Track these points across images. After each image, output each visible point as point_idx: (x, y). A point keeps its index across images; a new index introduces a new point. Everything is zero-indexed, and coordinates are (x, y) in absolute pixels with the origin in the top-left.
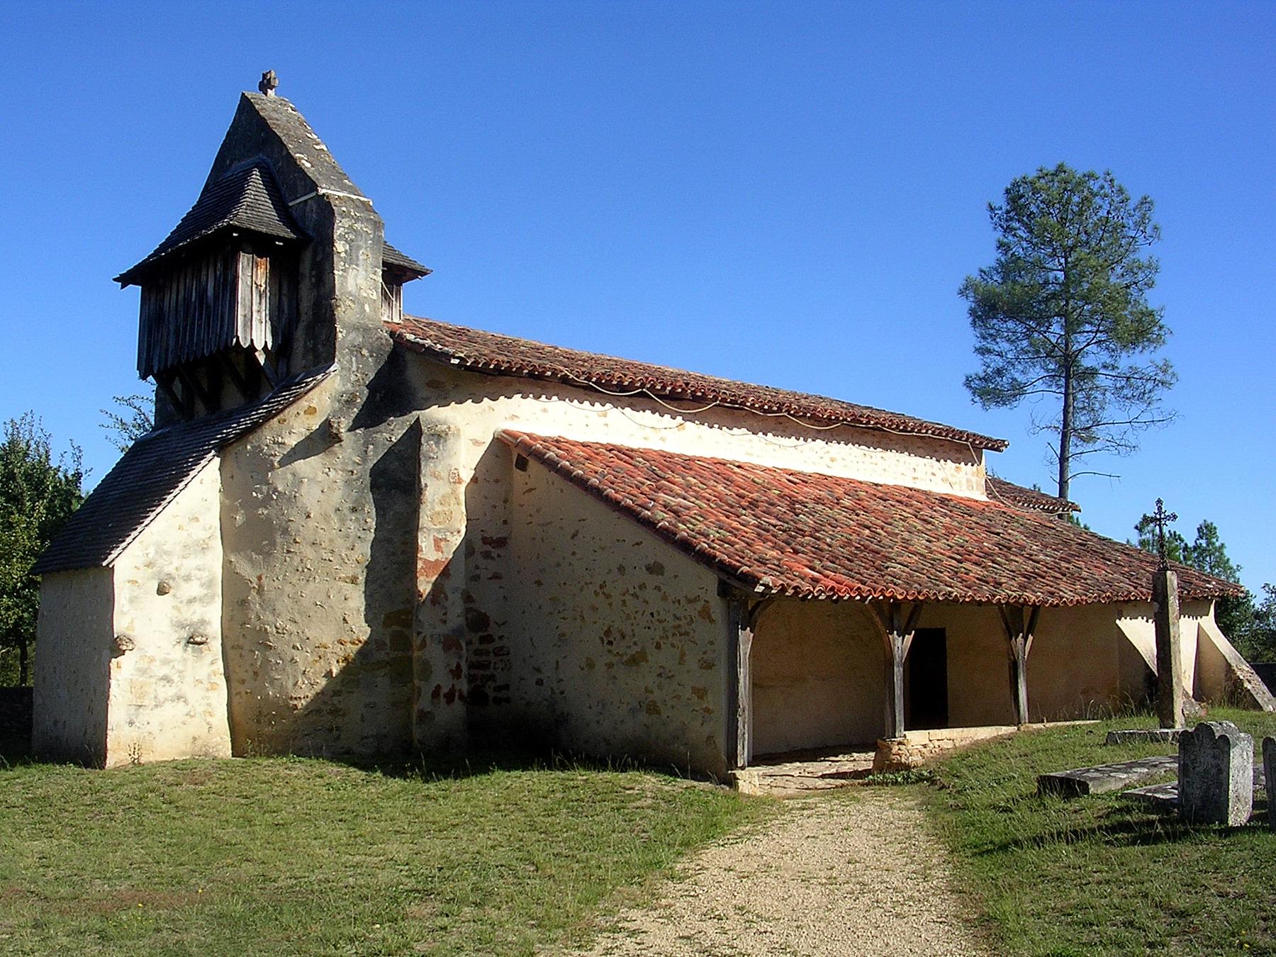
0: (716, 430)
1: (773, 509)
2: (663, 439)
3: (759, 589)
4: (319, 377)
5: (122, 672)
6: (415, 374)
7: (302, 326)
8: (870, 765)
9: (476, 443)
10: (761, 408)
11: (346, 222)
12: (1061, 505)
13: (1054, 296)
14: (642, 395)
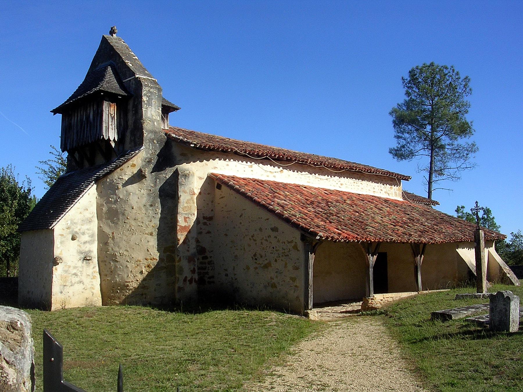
0: (296, 172)
1: (320, 205)
2: (274, 176)
3: (318, 238)
4: (137, 152)
5: (58, 272)
6: (176, 150)
7: (129, 131)
8: (360, 308)
9: (201, 178)
10: (314, 164)
11: (147, 89)
12: (429, 201)
13: (427, 116)
14: (267, 159)
